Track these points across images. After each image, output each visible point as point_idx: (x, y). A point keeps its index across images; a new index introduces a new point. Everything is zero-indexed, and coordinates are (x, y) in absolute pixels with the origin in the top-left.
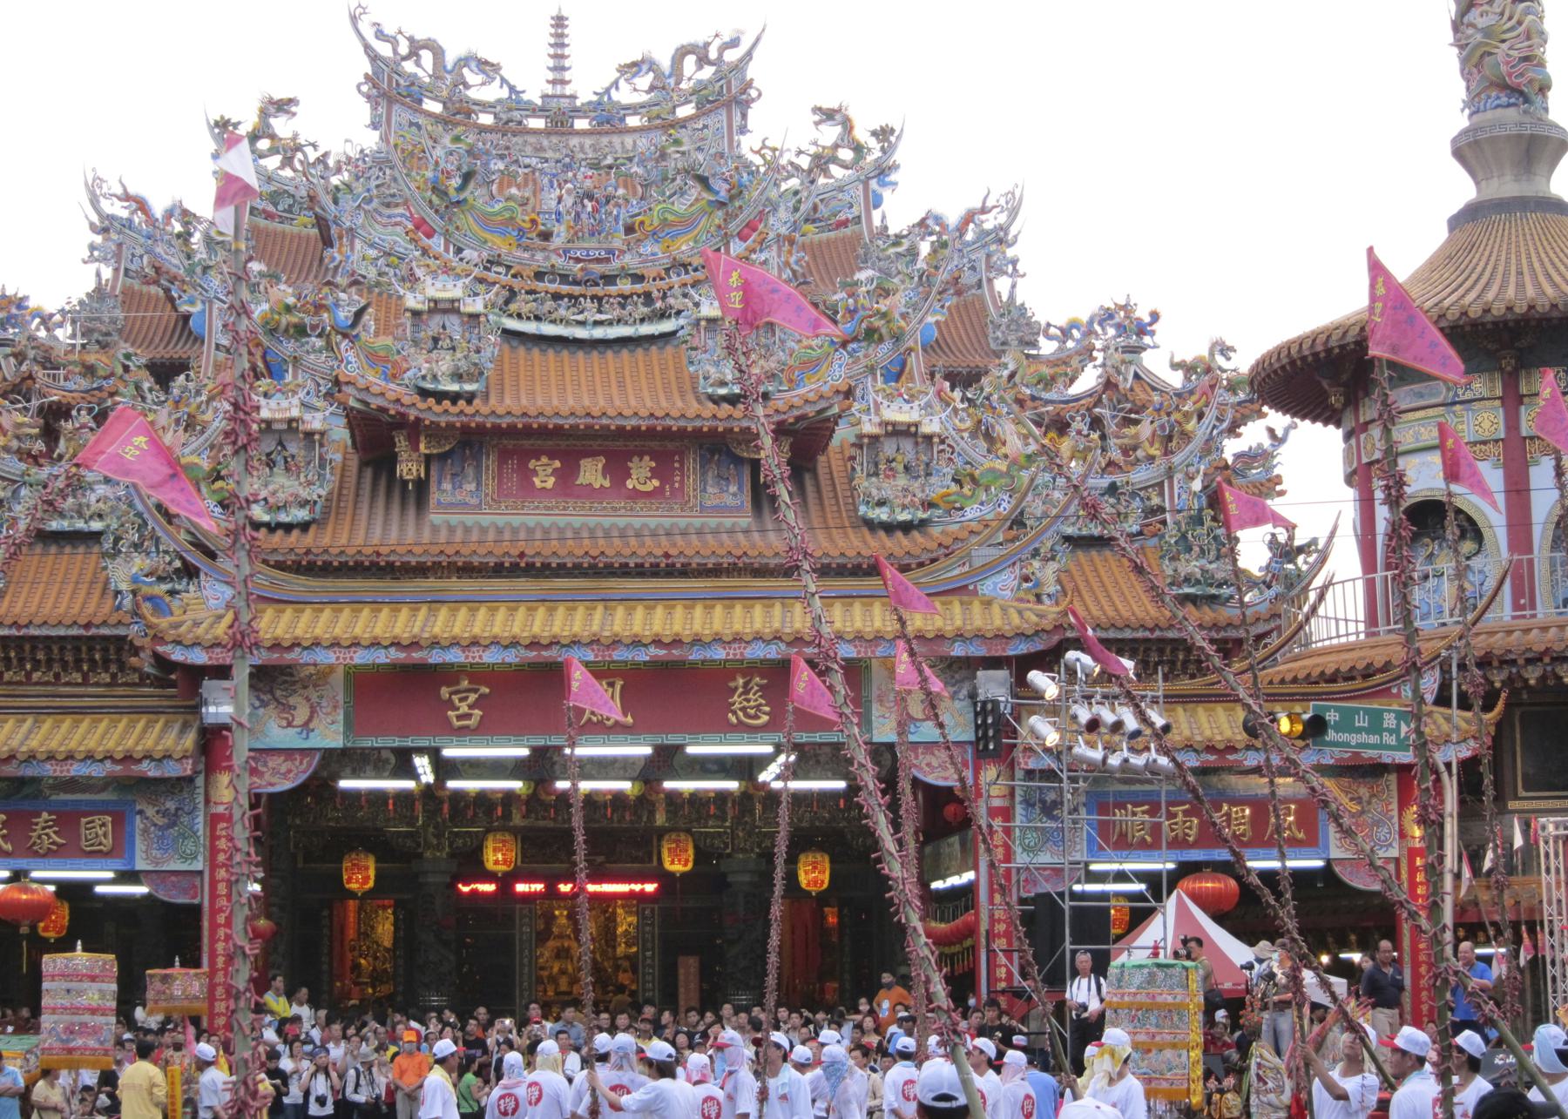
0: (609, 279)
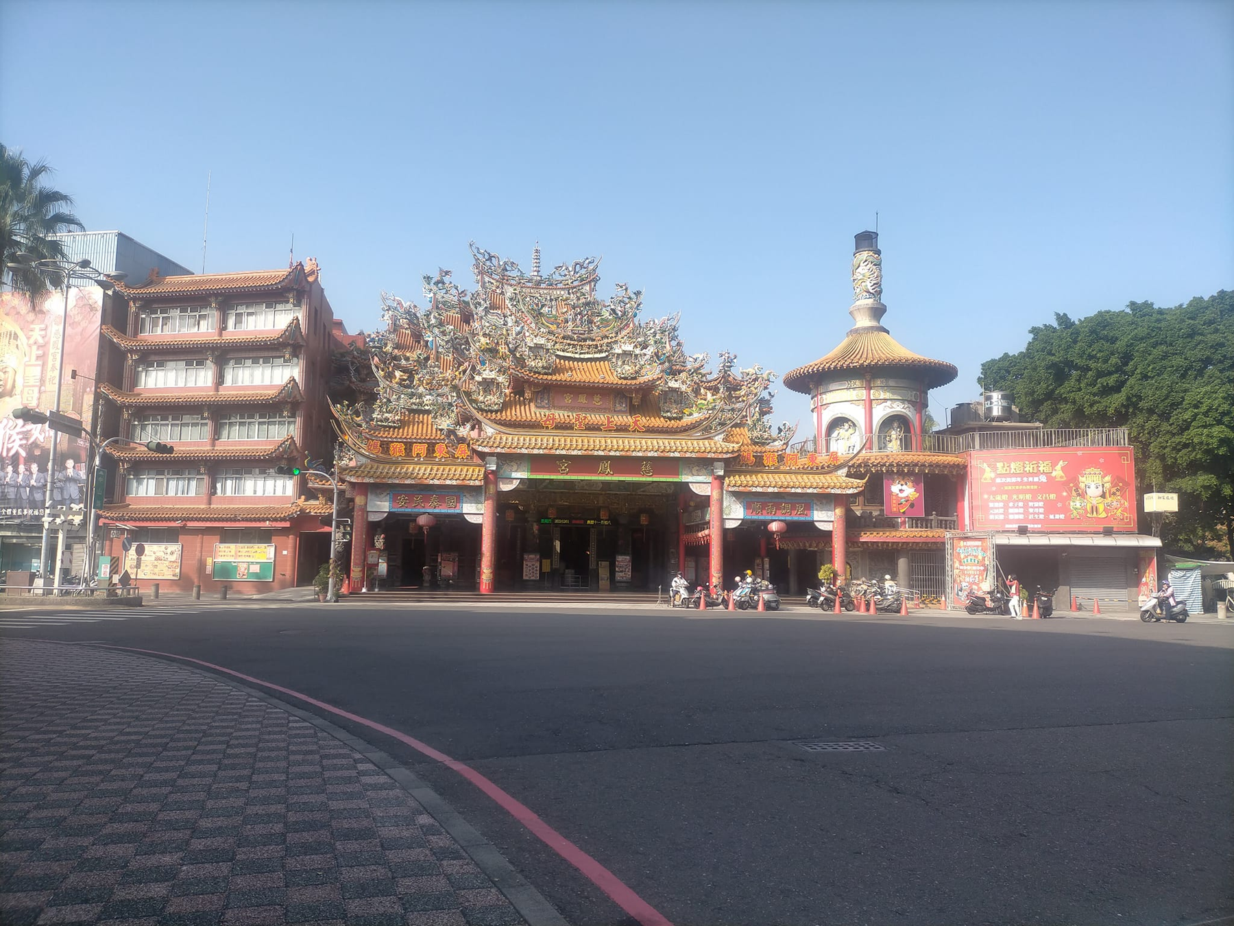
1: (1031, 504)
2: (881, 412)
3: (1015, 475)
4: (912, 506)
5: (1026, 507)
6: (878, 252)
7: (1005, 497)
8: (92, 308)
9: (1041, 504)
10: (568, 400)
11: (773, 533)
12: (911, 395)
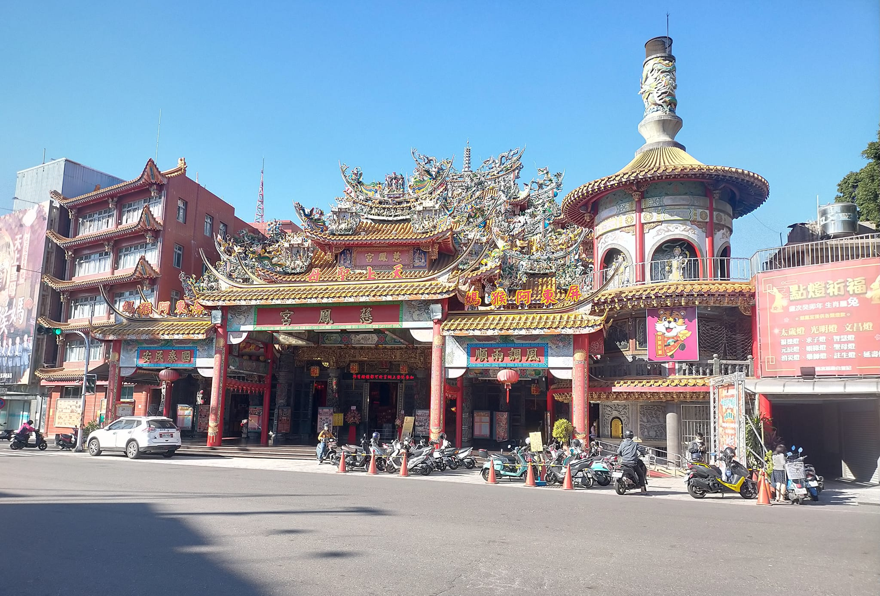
0: (400, 203)
1: (836, 338)
2: (653, 240)
3: (813, 300)
4: (683, 347)
5: (829, 342)
6: (671, 58)
7: (801, 330)
8: (44, 219)
9: (851, 337)
10: (369, 258)
11: (503, 383)
12: (698, 213)
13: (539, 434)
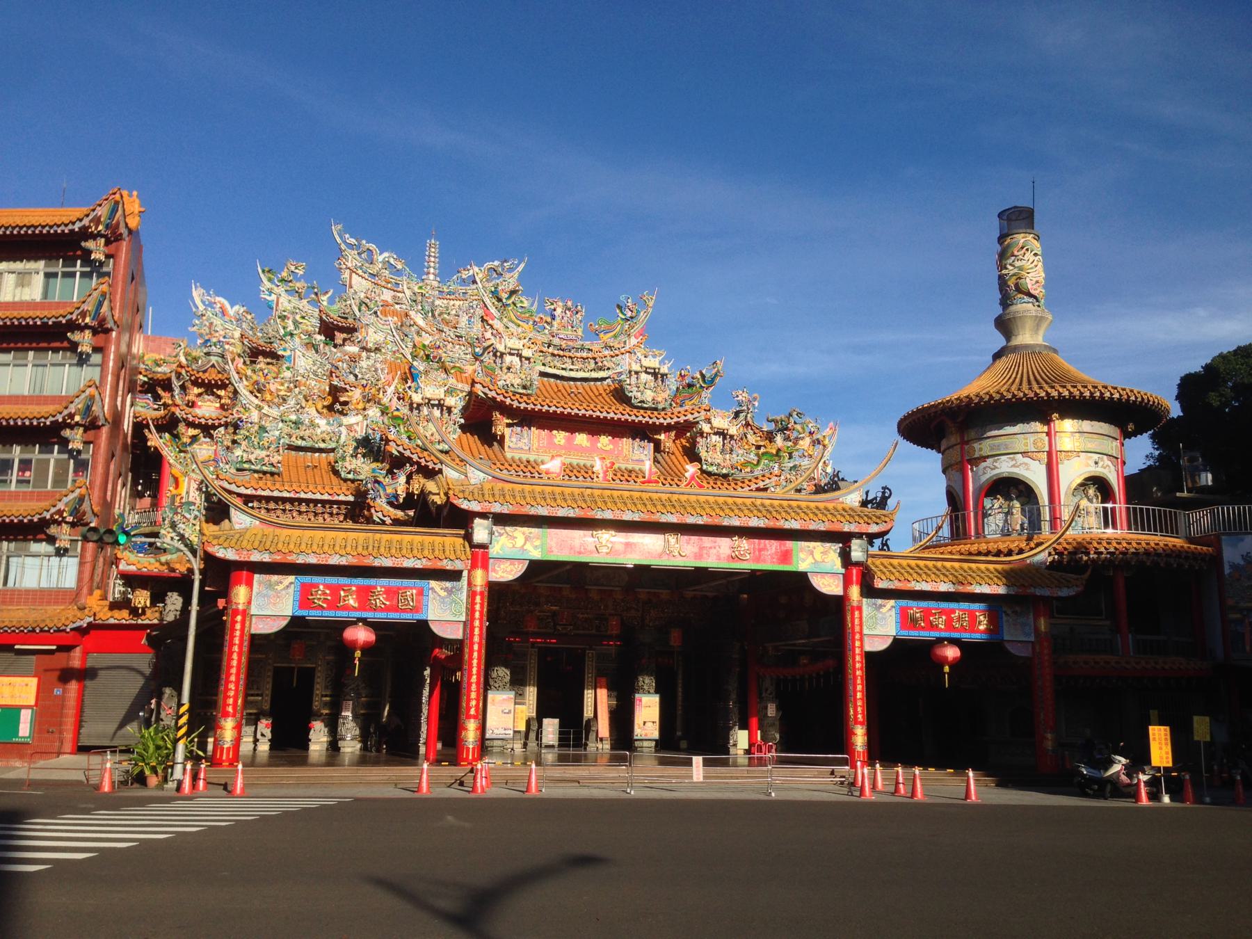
13: (557, 721)
